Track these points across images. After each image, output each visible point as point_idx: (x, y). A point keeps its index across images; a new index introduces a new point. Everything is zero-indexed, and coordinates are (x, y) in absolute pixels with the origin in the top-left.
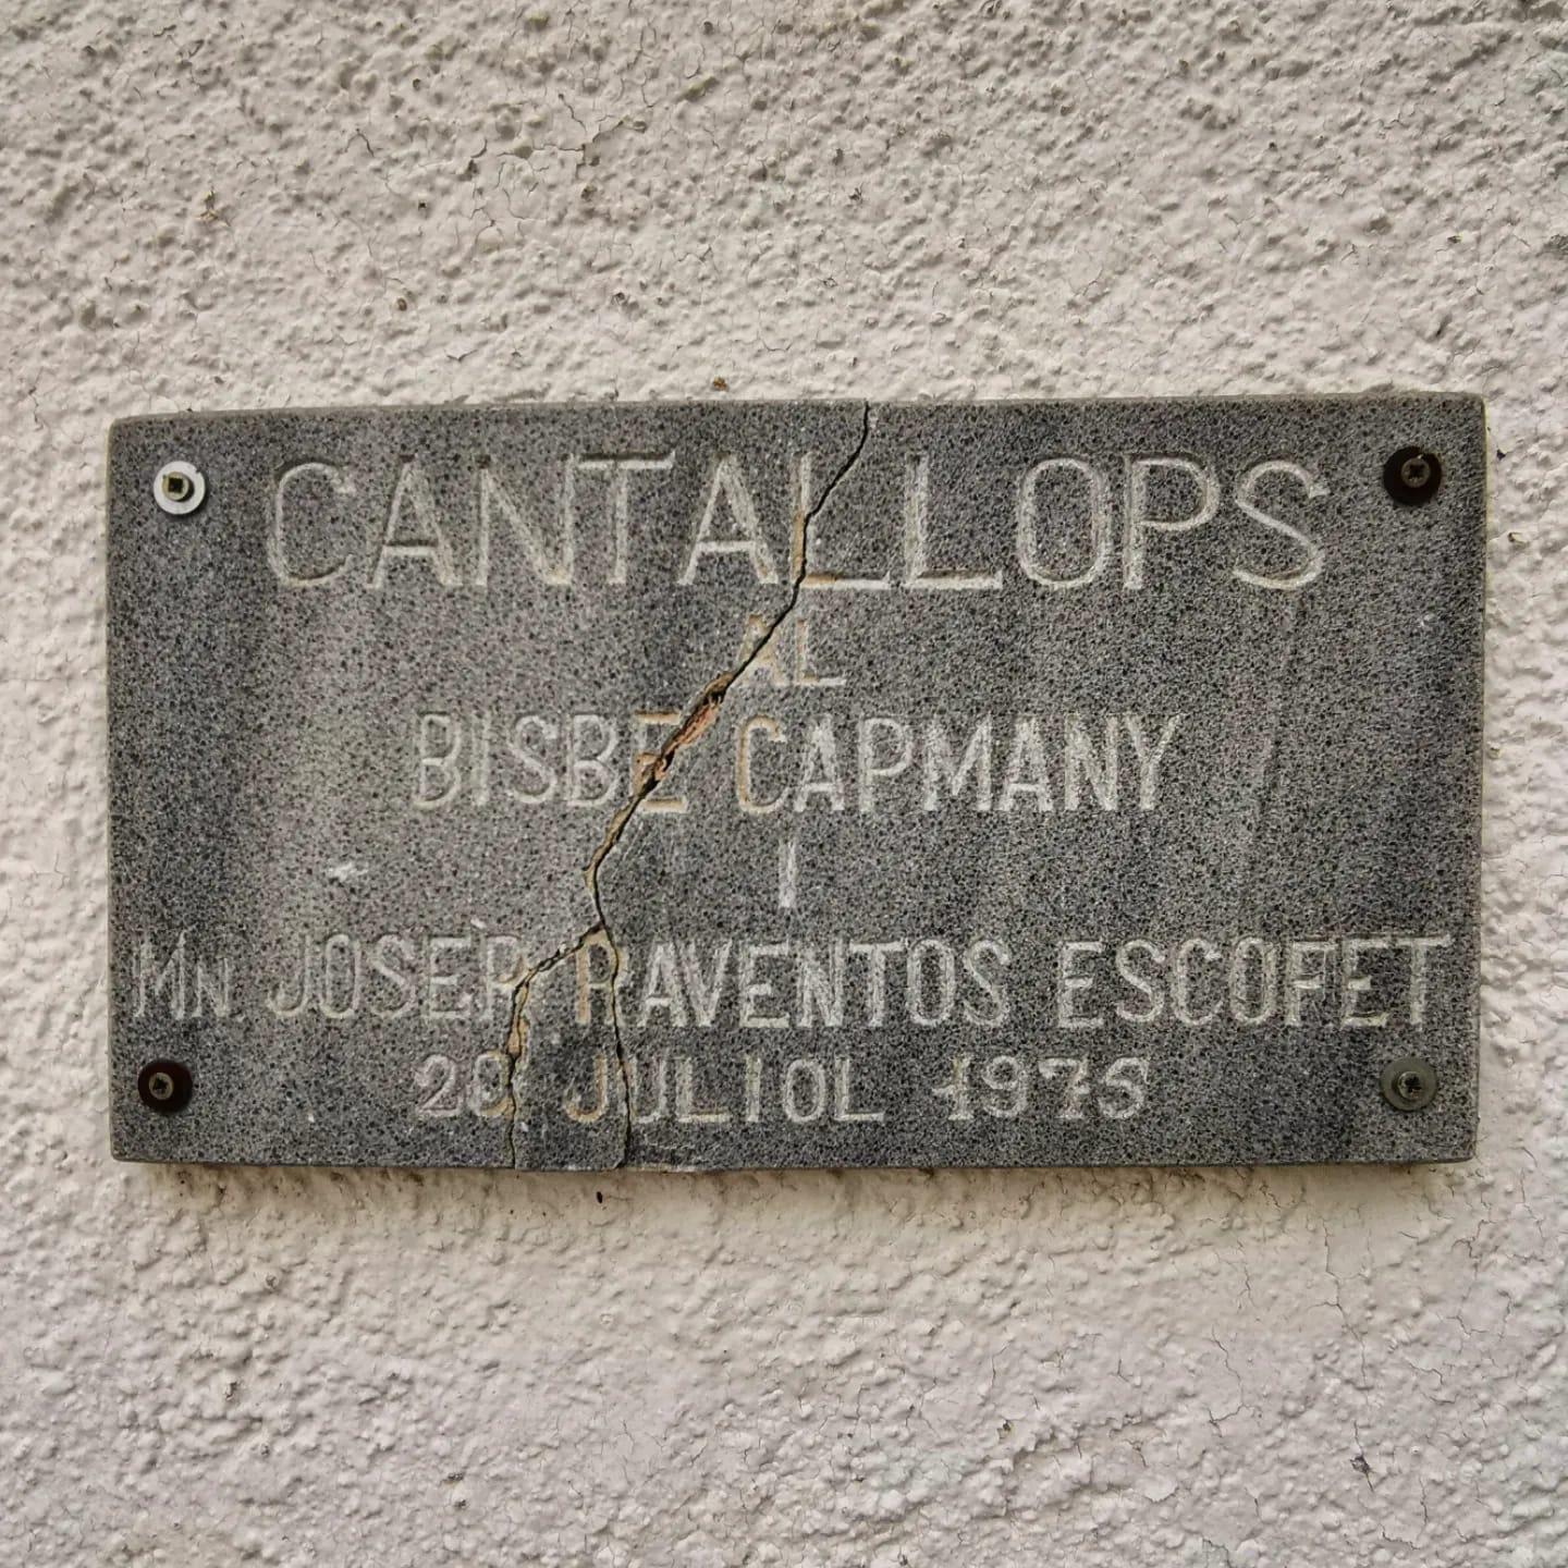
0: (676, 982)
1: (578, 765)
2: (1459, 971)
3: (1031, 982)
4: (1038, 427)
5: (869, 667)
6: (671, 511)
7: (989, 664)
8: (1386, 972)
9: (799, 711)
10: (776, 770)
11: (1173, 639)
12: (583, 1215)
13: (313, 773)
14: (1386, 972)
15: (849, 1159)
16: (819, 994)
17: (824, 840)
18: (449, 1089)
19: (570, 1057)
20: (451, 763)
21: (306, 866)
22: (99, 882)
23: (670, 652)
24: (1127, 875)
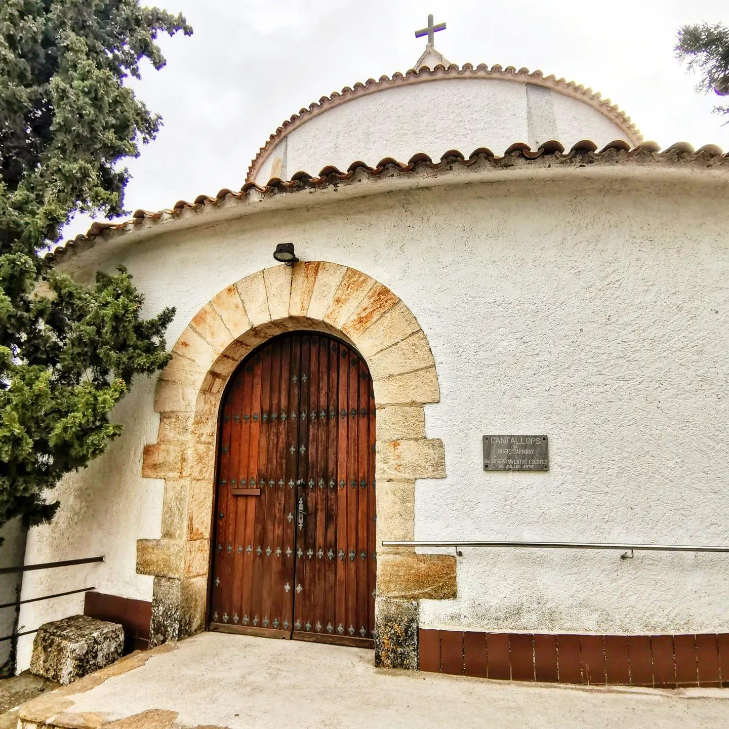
0: (511, 461)
1: (506, 451)
2: (548, 462)
3: (528, 462)
4: (527, 436)
5: (520, 447)
6: (510, 440)
7: (525, 447)
8: (544, 461)
9: (516, 449)
10: (515, 452)
11: (534, 446)
12: (541, 93)
13: (493, 451)
14: (544, 461)
15: (519, 470)
16: (518, 462)
17: (518, 455)
18: (500, 466)
19: (506, 465)
20: (500, 451)
21: (493, 456)
22: (382, 407)
23: (510, 446)
24: (532, 457)
